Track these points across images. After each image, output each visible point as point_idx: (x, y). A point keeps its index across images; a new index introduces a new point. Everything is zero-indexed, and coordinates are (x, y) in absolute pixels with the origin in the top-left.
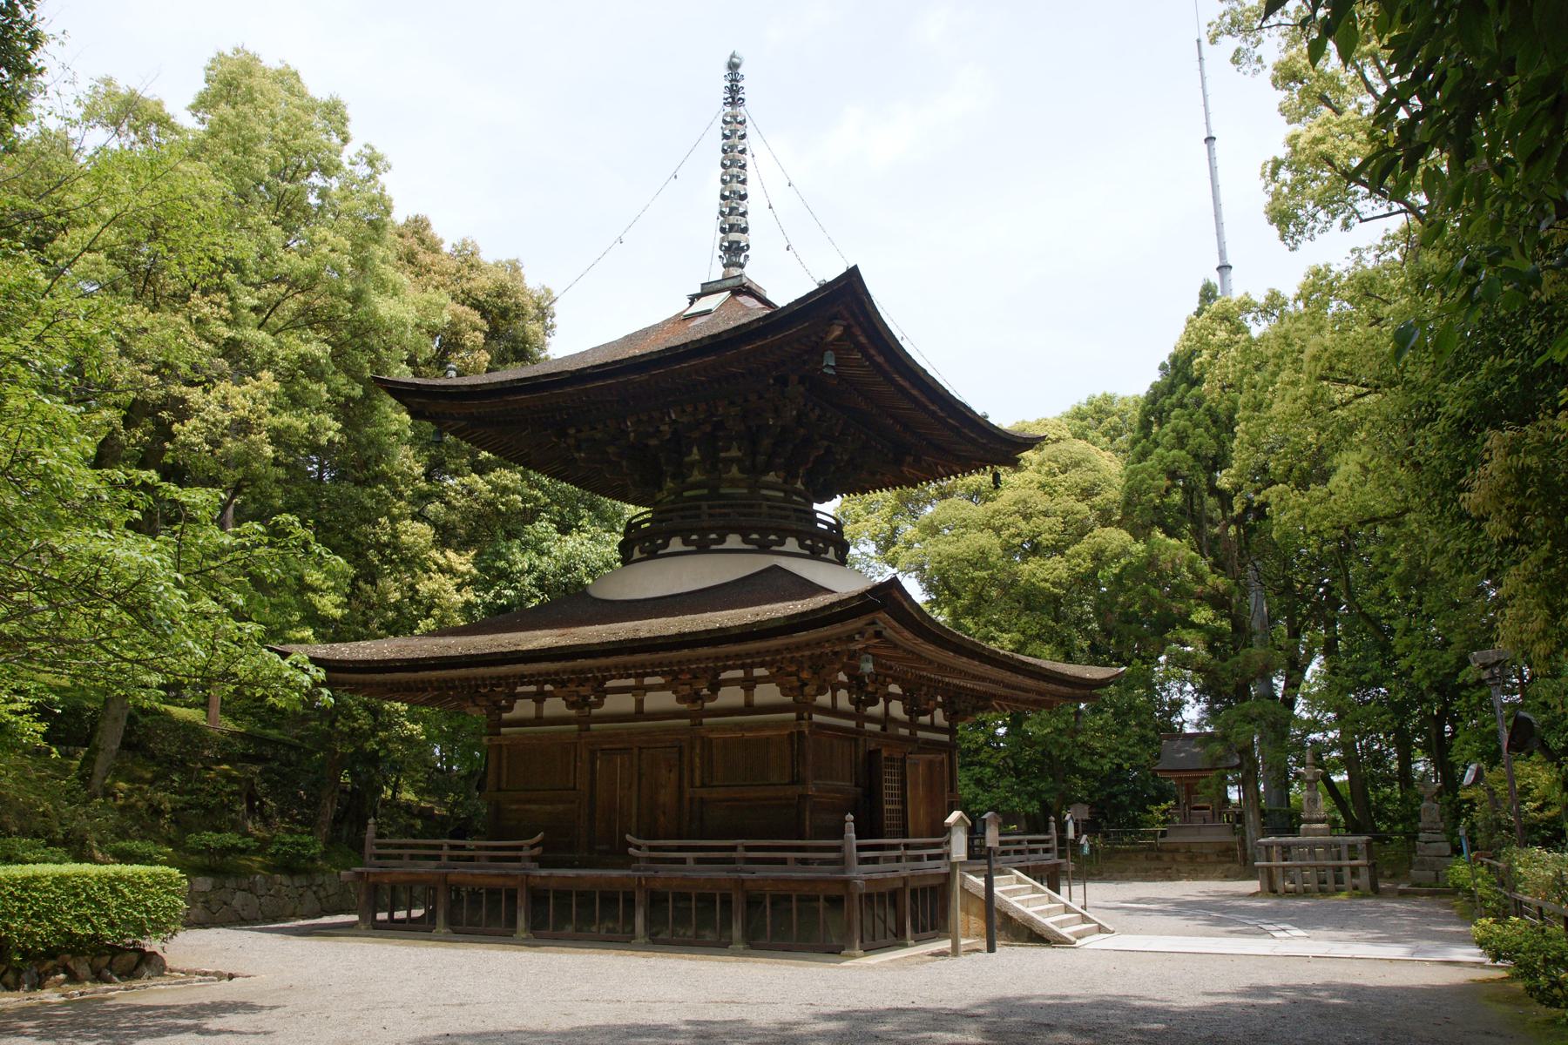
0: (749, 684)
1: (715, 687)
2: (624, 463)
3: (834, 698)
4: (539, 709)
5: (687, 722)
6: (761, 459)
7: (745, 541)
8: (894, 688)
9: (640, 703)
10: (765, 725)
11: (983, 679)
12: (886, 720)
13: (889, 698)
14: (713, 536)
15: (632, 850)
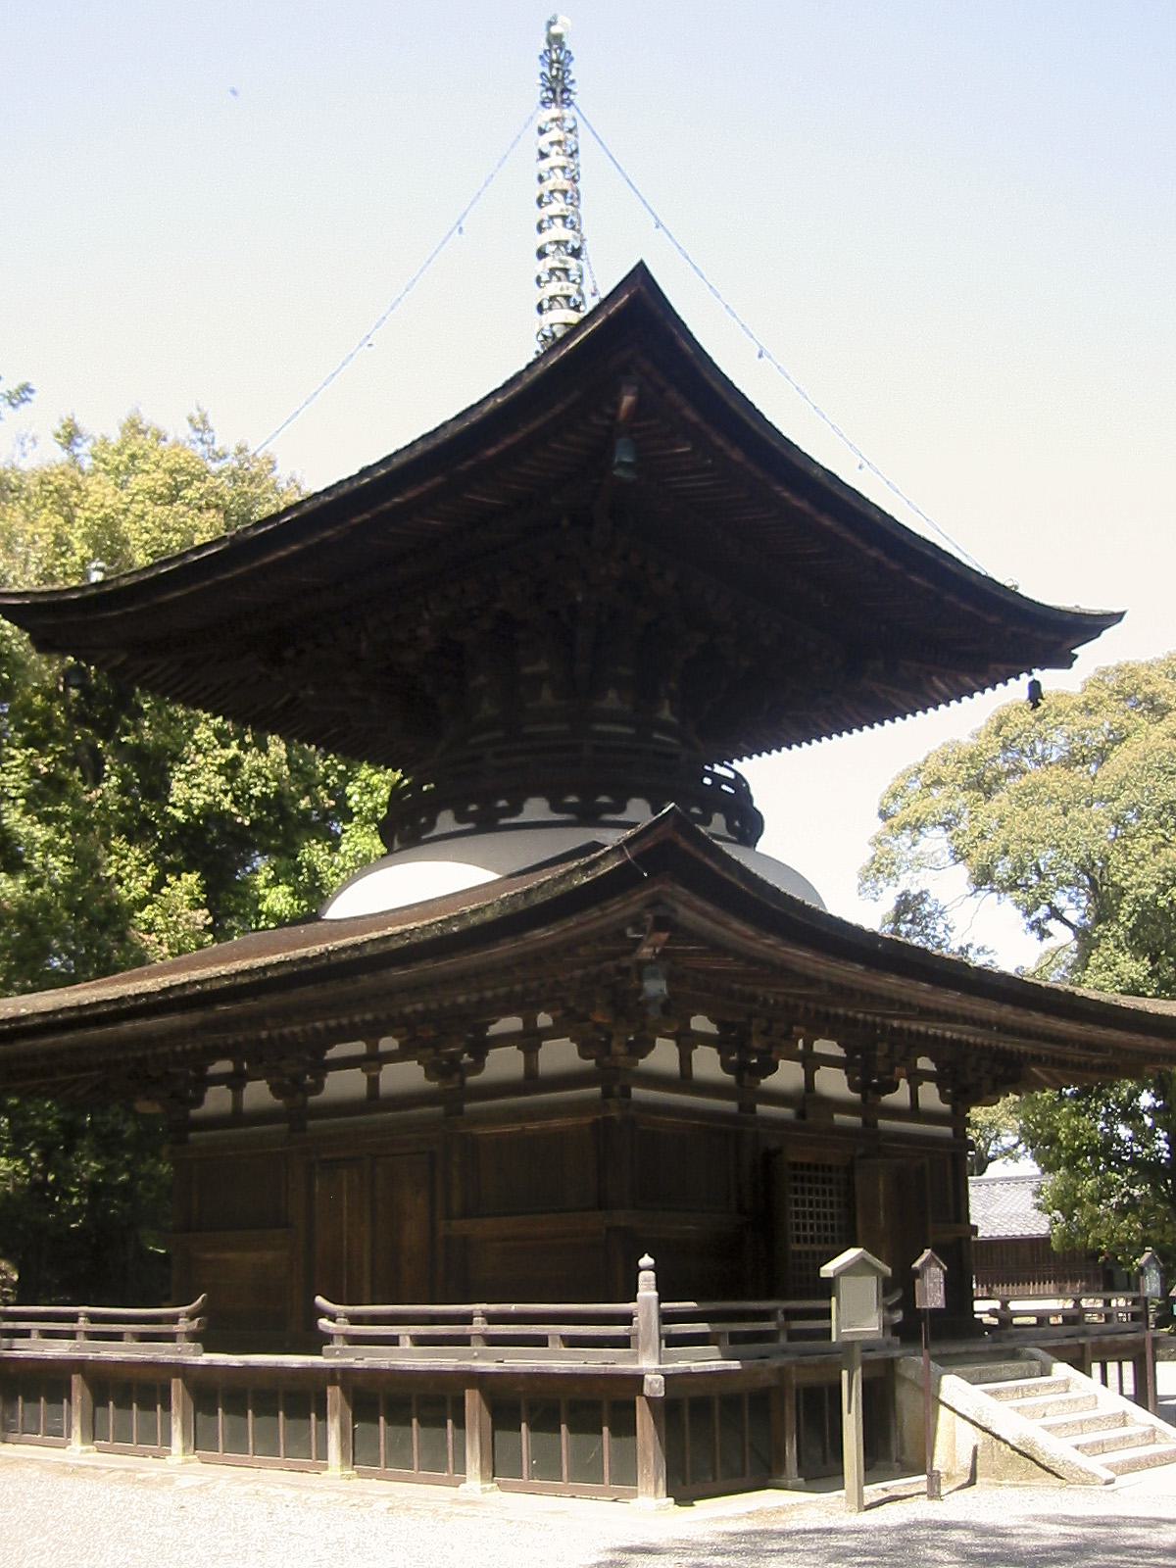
0: (529, 1041)
1: (481, 1047)
3: (685, 1060)
4: (237, 1099)
5: (439, 1109)
7: (556, 807)
8: (924, 1063)
9: (373, 1083)
10: (553, 1110)
11: (948, 1017)
12: (808, 1099)
13: (916, 1078)
14: (502, 803)
15: (324, 1322)
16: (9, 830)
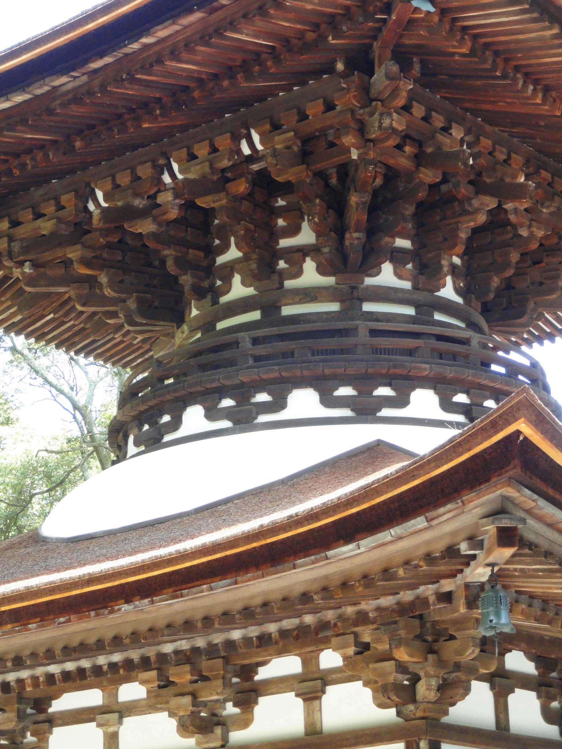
0: (311, 685)
1: (248, 695)
2: (103, 279)
3: (501, 709)
6: (354, 238)
7: (328, 400)
16: (412, 275)
